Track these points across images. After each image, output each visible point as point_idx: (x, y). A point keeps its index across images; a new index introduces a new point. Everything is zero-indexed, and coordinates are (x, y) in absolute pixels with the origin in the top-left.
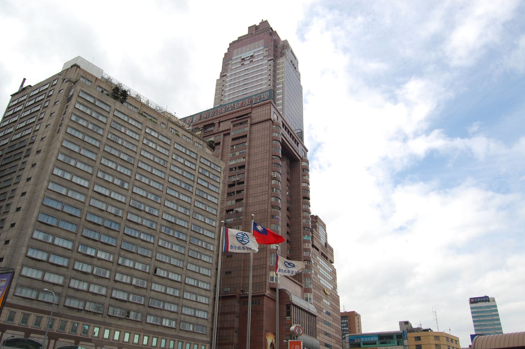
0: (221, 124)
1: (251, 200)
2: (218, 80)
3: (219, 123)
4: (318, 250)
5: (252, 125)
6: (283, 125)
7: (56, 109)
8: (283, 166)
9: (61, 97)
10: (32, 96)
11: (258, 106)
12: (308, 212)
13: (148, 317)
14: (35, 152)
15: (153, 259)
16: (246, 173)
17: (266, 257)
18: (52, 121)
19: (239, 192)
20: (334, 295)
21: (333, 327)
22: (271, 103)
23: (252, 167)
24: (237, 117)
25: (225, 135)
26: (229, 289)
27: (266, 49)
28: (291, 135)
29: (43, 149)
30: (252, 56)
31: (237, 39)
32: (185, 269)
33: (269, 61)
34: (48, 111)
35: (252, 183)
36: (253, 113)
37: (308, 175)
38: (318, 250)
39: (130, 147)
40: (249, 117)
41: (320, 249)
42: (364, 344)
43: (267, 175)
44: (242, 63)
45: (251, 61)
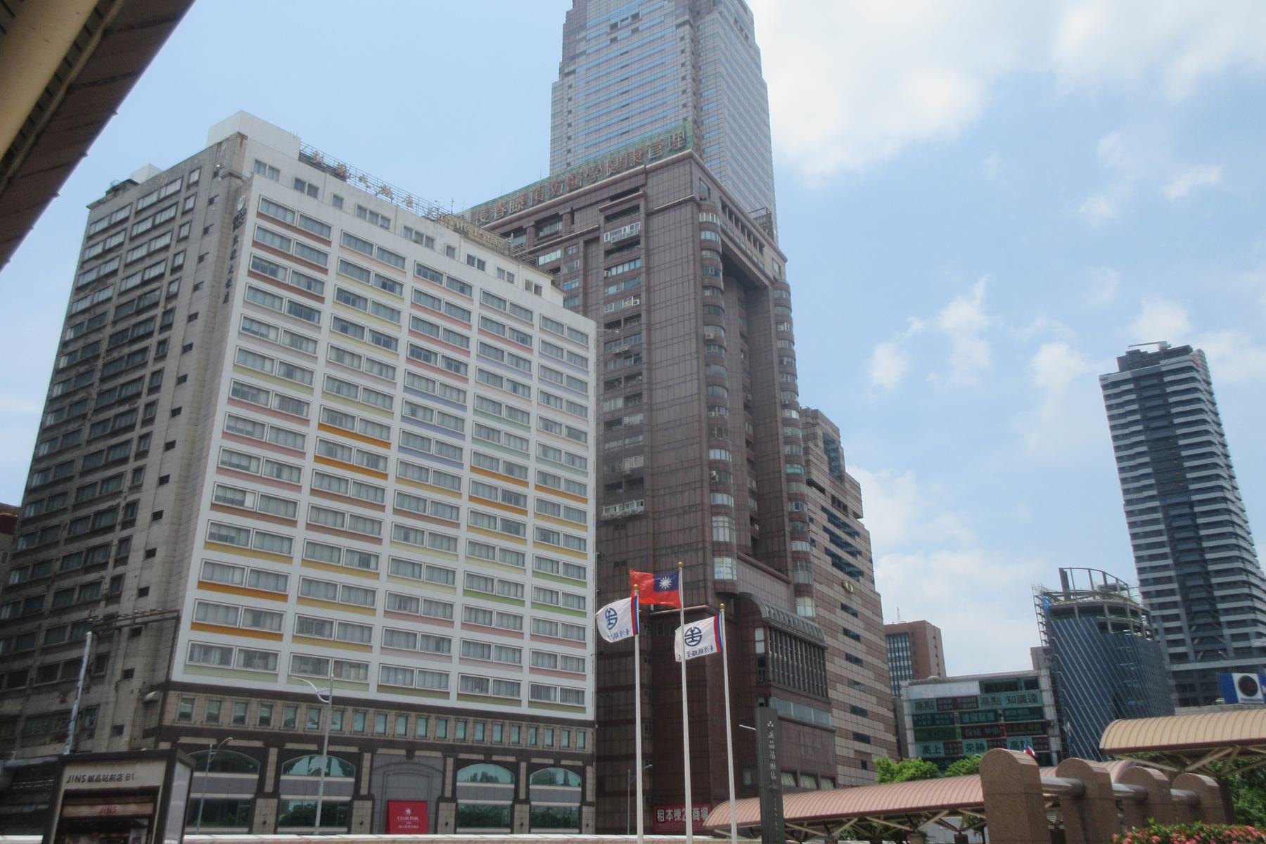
0: (577, 216)
1: (659, 396)
3: (572, 213)
4: (822, 490)
5: (649, 215)
6: (724, 207)
7: (211, 244)
8: (730, 305)
9: (216, 216)
10: (144, 209)
11: (661, 167)
12: (793, 405)
14: (179, 349)
16: (644, 332)
17: (703, 525)
18: (207, 275)
20: (868, 592)
21: (871, 667)
23: (657, 317)
24: (613, 198)
25: (587, 243)
28: (743, 228)
29: (195, 340)
30: (635, 17)
33: (678, 26)
34: (193, 252)
35: (659, 355)
36: (650, 184)
37: (789, 321)
38: (822, 490)
40: (639, 197)
43: (694, 335)
44: (613, 36)
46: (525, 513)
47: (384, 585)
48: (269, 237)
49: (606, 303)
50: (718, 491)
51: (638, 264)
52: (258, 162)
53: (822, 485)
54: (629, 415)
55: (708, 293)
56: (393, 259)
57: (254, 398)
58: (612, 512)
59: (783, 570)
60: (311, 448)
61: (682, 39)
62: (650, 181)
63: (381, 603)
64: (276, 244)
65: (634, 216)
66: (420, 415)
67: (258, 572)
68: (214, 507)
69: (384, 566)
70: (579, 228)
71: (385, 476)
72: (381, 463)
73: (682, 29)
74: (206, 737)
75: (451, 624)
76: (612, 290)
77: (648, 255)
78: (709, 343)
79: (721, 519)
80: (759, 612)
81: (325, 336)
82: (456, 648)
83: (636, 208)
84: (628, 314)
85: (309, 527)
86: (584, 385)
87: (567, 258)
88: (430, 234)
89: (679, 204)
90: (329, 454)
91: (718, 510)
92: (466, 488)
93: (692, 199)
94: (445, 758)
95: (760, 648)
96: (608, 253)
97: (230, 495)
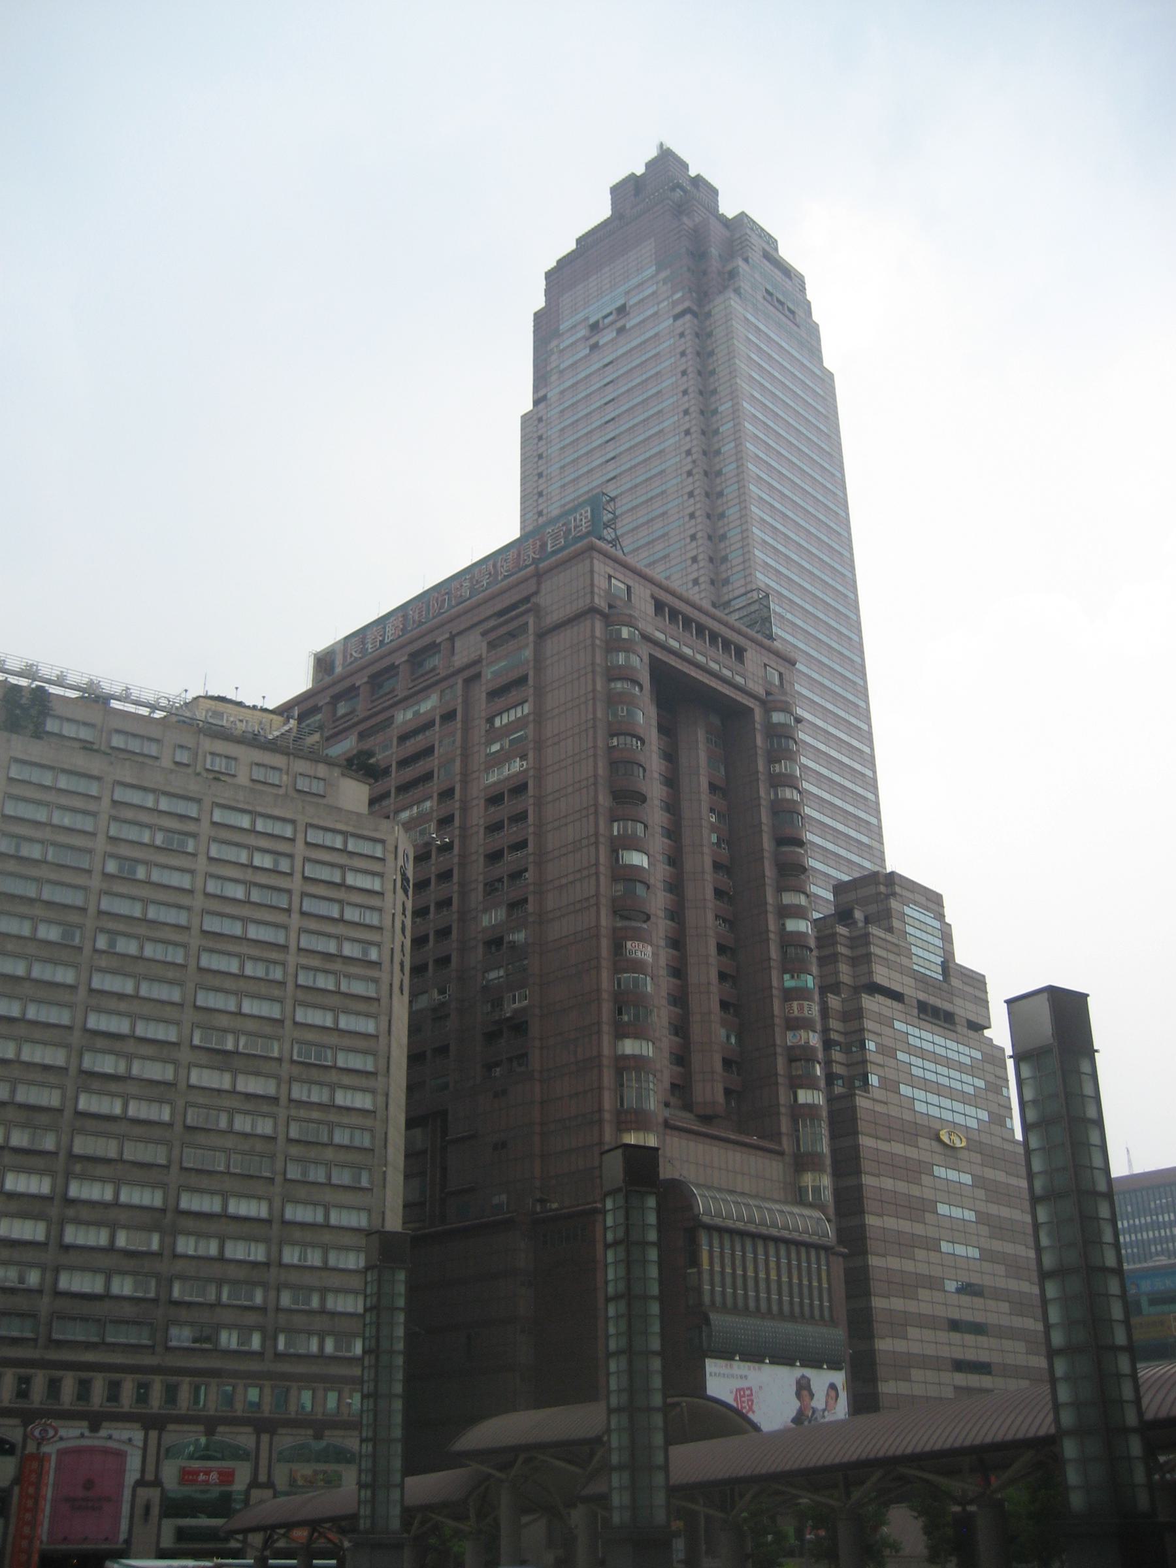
0: (458, 644)
2: (526, 420)
3: (452, 639)
4: (897, 996)
5: (541, 636)
13: (174, 1331)
15: (175, 1169)
19: (516, 875)
22: (592, 548)
24: (500, 614)
25: (468, 681)
26: (504, 1197)
27: (663, 275)
30: (622, 310)
31: (573, 246)
32: (279, 1179)
33: (676, 317)
38: (897, 996)
39: (70, 859)
41: (907, 991)
42: (1153, 1302)
44: (592, 341)
45: (621, 330)
51: (527, 708)
53: (897, 988)
61: (682, 335)
73: (680, 322)
74: (189, 1423)
77: (540, 692)
83: (524, 627)
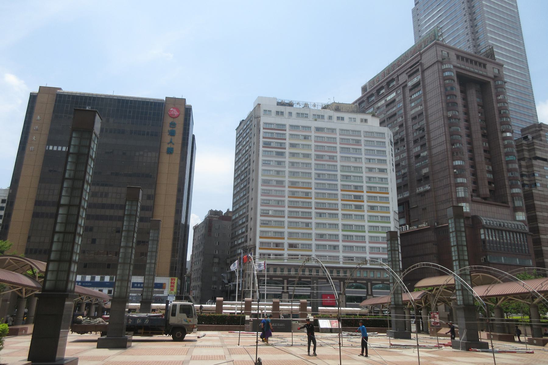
1: (433, 143)
3: (398, 76)
5: (423, 72)
24: (411, 67)
46: (363, 201)
47: (314, 231)
48: (267, 134)
49: (411, 110)
50: (458, 177)
52: (265, 111)
54: (422, 152)
55: (449, 98)
56: (307, 129)
57: (269, 183)
58: (420, 190)
59: (506, 202)
60: (287, 194)
62: (423, 58)
63: (314, 237)
64: (270, 136)
65: (418, 73)
66: (321, 177)
67: (275, 232)
68: (261, 216)
69: (314, 226)
70: (400, 82)
71: (311, 198)
72: (310, 194)
75: (338, 241)
76: (413, 104)
78: (449, 118)
79: (460, 188)
80: (481, 223)
81: (287, 159)
82: (341, 248)
84: (419, 113)
85: (289, 217)
86: (384, 152)
87: (398, 95)
88: (322, 114)
89: (433, 64)
90: (293, 194)
91: (458, 185)
92: (340, 197)
93: (438, 61)
94: (340, 282)
95: (483, 237)
96: (411, 90)
97: (265, 212)
